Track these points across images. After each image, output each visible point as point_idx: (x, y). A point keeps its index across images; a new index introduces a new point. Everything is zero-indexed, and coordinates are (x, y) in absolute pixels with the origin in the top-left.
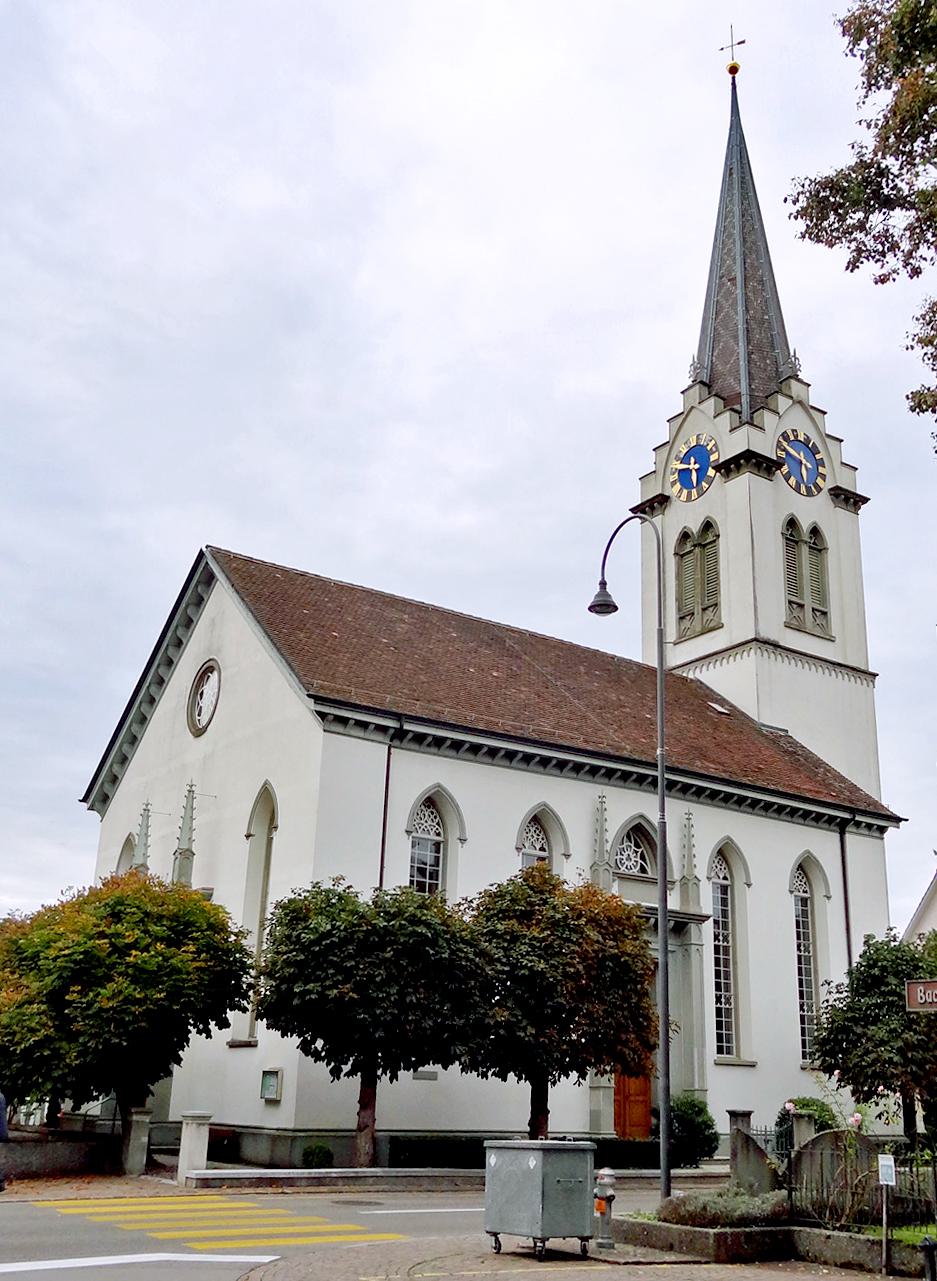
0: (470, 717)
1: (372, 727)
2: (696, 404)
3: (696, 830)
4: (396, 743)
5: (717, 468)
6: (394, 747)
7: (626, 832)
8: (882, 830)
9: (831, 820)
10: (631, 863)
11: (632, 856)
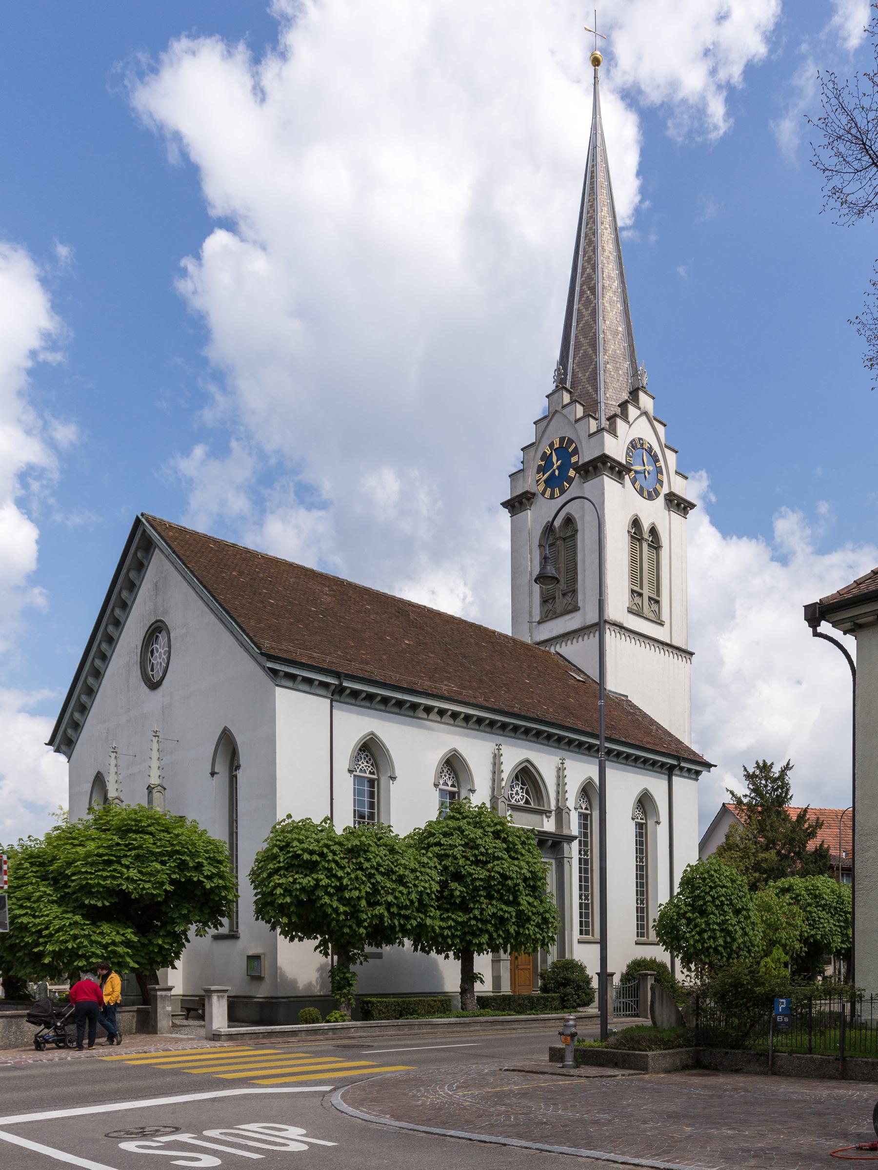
0: (394, 677)
1: (300, 678)
2: (559, 409)
3: (566, 773)
4: (336, 697)
5: (577, 469)
6: (336, 701)
7: (514, 775)
8: (698, 773)
9: (663, 765)
10: (519, 796)
11: (520, 791)
